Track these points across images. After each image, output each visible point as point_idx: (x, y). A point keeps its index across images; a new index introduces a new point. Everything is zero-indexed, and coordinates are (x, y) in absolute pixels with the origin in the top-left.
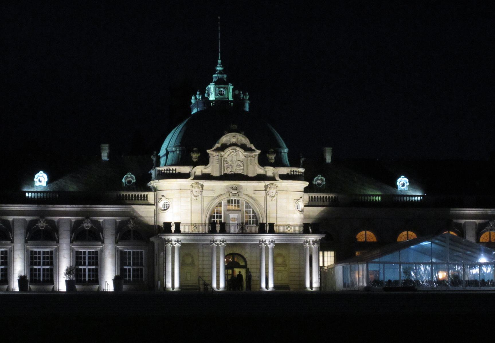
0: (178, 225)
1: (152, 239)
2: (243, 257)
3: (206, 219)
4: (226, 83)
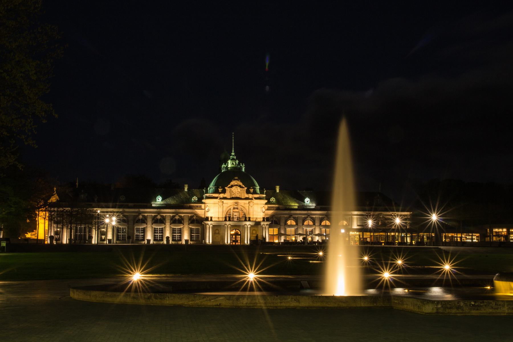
0: (211, 218)
4: (235, 160)
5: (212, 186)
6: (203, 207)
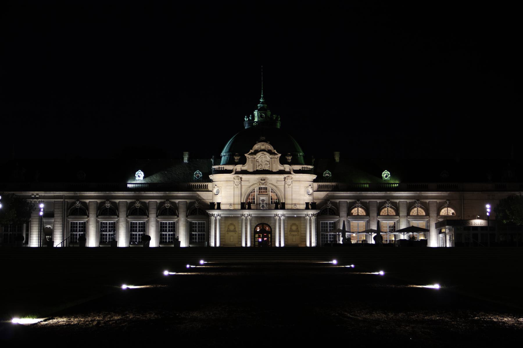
0: (219, 204)
5: (224, 154)
6: (210, 188)
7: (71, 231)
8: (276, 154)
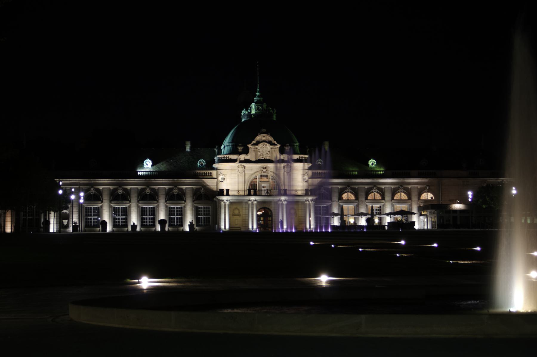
1: (215, 199)
2: (271, 211)
3: (247, 187)
7: (87, 215)
8: (275, 145)
